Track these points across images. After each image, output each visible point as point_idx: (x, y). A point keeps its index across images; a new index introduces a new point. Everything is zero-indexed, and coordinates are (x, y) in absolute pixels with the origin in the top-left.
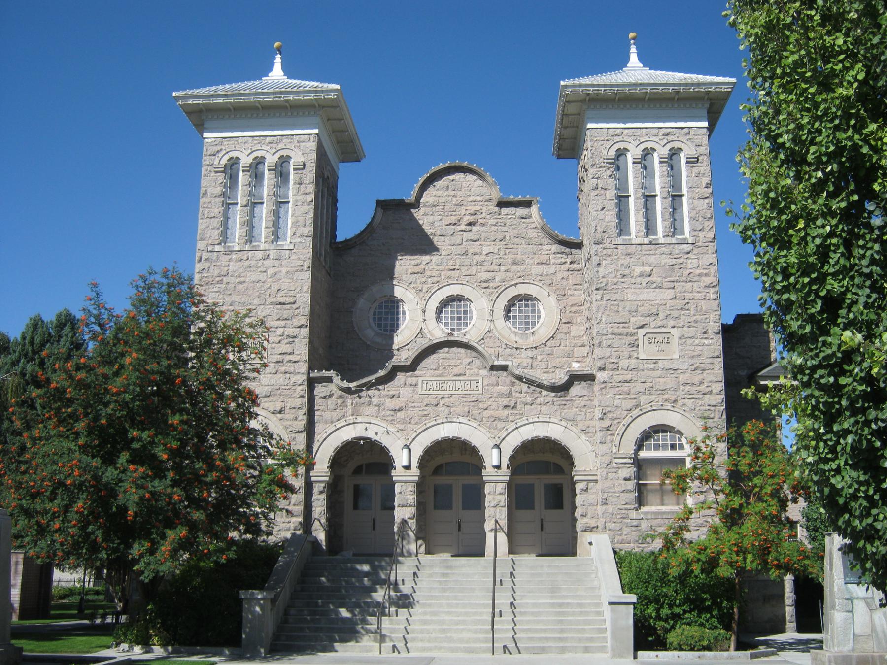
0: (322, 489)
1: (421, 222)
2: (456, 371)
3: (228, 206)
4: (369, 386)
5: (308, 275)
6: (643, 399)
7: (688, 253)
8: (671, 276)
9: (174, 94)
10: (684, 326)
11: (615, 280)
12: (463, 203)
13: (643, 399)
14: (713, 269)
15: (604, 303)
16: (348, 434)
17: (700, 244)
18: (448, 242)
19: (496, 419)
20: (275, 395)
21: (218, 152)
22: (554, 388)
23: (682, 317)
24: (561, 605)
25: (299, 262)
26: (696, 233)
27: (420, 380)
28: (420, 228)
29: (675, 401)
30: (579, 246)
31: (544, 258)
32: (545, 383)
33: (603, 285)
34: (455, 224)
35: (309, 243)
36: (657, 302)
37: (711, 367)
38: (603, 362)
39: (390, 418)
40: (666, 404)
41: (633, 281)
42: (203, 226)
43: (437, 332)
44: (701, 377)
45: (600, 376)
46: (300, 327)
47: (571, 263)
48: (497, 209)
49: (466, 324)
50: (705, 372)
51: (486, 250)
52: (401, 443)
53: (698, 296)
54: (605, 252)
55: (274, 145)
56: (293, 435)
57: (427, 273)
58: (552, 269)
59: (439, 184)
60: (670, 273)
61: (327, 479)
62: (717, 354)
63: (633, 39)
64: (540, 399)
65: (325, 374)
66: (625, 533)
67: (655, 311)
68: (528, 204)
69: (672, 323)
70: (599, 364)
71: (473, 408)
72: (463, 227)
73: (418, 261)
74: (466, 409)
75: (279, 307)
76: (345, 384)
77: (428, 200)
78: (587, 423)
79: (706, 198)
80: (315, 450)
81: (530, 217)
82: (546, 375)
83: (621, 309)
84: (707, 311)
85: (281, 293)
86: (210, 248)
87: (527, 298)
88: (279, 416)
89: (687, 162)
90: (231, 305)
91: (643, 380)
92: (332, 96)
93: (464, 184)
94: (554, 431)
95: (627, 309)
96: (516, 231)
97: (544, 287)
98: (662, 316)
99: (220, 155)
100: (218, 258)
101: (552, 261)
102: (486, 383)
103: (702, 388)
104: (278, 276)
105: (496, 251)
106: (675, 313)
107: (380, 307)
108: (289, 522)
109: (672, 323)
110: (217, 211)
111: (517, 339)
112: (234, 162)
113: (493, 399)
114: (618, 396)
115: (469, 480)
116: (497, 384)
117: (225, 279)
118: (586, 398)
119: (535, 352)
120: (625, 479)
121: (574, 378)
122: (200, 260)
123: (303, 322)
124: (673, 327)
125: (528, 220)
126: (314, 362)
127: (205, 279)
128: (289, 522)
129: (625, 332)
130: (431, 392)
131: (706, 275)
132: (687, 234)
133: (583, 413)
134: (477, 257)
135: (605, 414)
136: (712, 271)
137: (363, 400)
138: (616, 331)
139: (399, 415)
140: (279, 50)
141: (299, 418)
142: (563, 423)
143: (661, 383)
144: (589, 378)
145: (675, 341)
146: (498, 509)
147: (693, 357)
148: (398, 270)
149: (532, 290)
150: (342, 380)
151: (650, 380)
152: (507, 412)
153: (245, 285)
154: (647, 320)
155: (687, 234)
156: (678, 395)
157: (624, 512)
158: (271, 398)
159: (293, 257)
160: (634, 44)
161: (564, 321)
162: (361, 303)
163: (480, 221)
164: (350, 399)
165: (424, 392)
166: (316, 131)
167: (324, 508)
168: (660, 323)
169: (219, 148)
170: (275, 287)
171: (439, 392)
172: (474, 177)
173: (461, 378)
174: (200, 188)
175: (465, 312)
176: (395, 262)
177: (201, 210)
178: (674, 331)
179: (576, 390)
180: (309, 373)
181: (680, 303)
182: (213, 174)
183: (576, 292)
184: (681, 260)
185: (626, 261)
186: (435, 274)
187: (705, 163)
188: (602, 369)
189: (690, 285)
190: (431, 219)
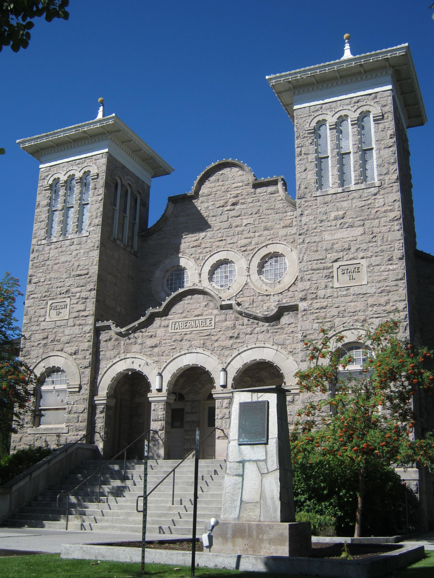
0: (101, 409)
1: (199, 208)
2: (196, 313)
3: (51, 212)
4: (135, 330)
6: (337, 321)
7: (375, 195)
8: (360, 216)
10: (371, 257)
11: (314, 226)
12: (229, 189)
13: (337, 321)
15: (306, 245)
16: (121, 367)
17: (385, 186)
18: (218, 220)
19: (224, 348)
20: (73, 342)
21: (47, 176)
22: (267, 319)
23: (371, 249)
25: (92, 244)
26: (381, 177)
27: (171, 321)
28: (198, 213)
29: (365, 321)
31: (288, 222)
32: (260, 315)
33: (305, 230)
34: (223, 206)
35: (99, 229)
36: (349, 239)
37: (395, 288)
38: (303, 293)
40: (357, 323)
44: (387, 298)
45: (302, 305)
46: (91, 290)
48: (253, 190)
50: (391, 293)
51: (245, 222)
52: (156, 371)
53: (384, 229)
54: (307, 204)
55: (80, 166)
56: (83, 370)
57: (203, 246)
59: (212, 179)
60: (359, 213)
61: (105, 402)
62: (400, 276)
63: (347, 39)
64: (258, 329)
65: (106, 323)
67: (346, 246)
68: (275, 183)
70: (301, 295)
71: (207, 342)
72: (229, 208)
73: (197, 237)
74: (202, 342)
75: (78, 278)
76: (119, 330)
77: (204, 191)
78: (294, 346)
79: (390, 147)
80: (99, 381)
84: (392, 241)
85: (80, 268)
86: (39, 243)
87: (276, 255)
88: (74, 356)
90: (50, 281)
91: (337, 305)
93: (230, 176)
94: (267, 354)
95: (324, 248)
96: (267, 205)
97: (288, 245)
98: (353, 250)
100: (43, 249)
102: (217, 320)
103: (388, 308)
104: (79, 256)
105: (252, 222)
106: (364, 246)
107: (172, 275)
108: (77, 435)
109: (361, 254)
110: (44, 216)
111: (267, 288)
112: (57, 180)
114: (317, 321)
116: (226, 320)
117: (47, 263)
118: (293, 325)
119: (281, 296)
121: (282, 310)
122: (33, 252)
123: (92, 287)
124: (363, 258)
126: (99, 316)
128: (77, 435)
129: (322, 267)
130: (178, 330)
131: (391, 211)
133: (291, 338)
134: (238, 229)
135: (305, 336)
136: (396, 207)
137: (133, 340)
138: (315, 267)
139: (156, 350)
140: (102, 103)
141: (87, 357)
142: (275, 347)
143: (352, 307)
144: (294, 308)
146: (224, 420)
147: (380, 282)
148: (183, 246)
149: (278, 248)
150: (117, 326)
151: (343, 305)
152: (232, 341)
153: (58, 265)
154: (341, 254)
158: (70, 344)
159: (89, 241)
160: (348, 42)
162: (158, 274)
163: (241, 201)
164: (123, 341)
165: (173, 331)
166: (106, 150)
167: (103, 424)
168: (351, 256)
170: (77, 264)
171: (183, 330)
172: (237, 169)
174: (36, 202)
175: (231, 272)
176: (181, 241)
177: (35, 217)
178: (364, 262)
179: (285, 319)
180: (95, 324)
181: (368, 237)
182: (44, 192)
184: (369, 202)
186: (208, 245)
188: (304, 299)
189: (377, 221)
190: (206, 205)
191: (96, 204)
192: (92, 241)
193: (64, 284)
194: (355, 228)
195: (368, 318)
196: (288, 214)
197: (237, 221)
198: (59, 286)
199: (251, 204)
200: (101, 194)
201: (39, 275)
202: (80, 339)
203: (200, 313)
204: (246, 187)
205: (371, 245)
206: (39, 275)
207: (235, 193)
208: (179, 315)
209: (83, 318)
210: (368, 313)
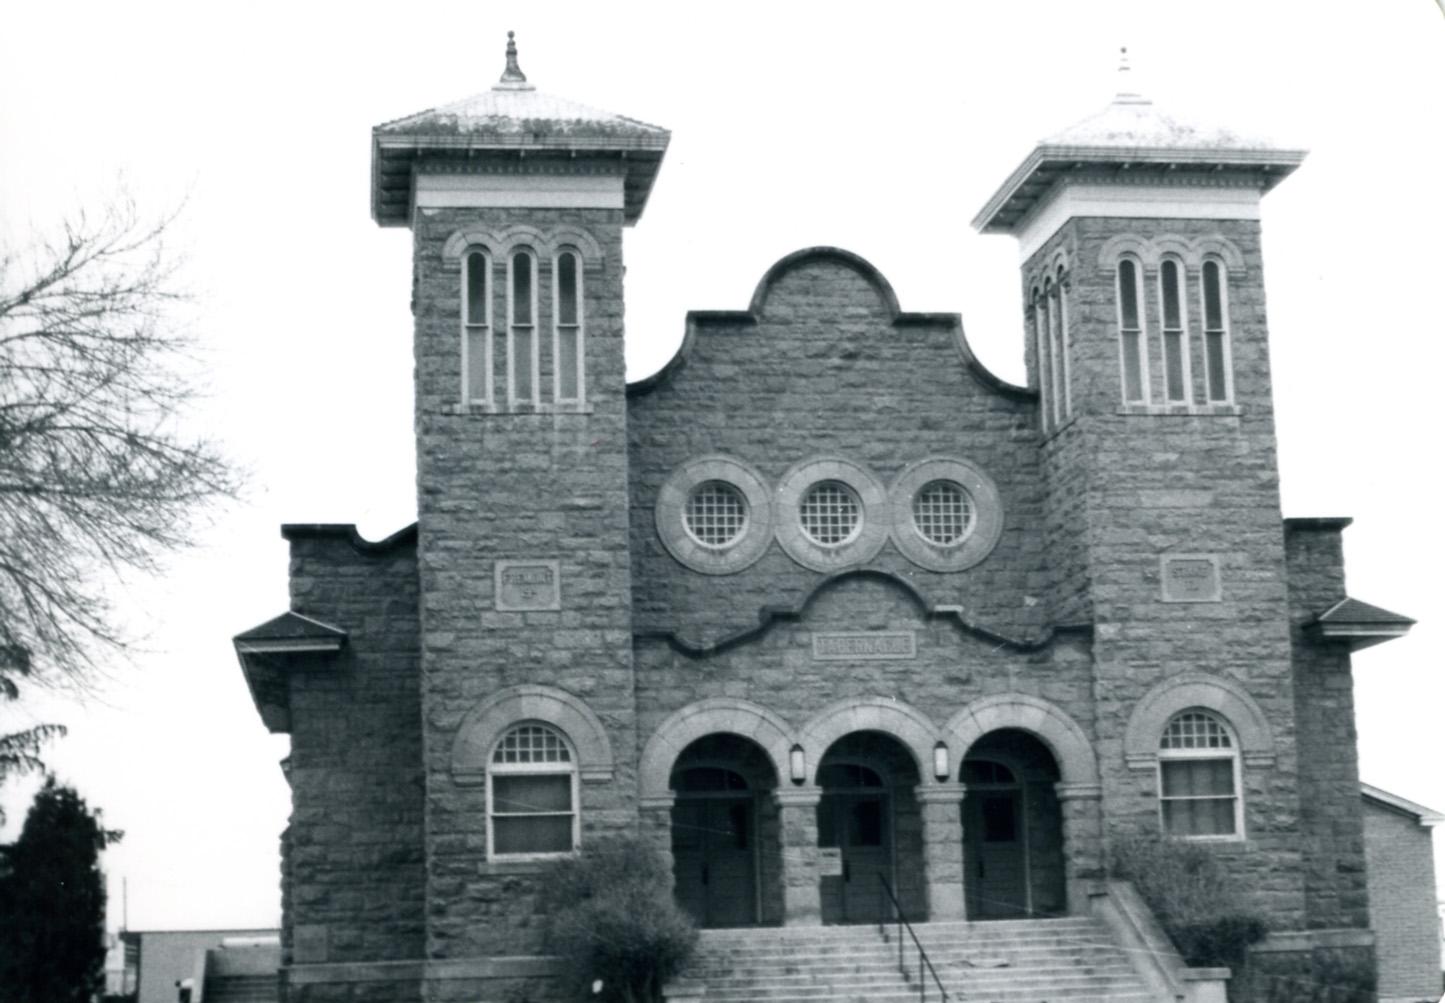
2: (874, 620)
22: (1026, 649)
27: (815, 636)
31: (976, 418)
48: (894, 332)
58: (988, 439)
69: (1212, 545)
72: (836, 361)
75: (576, 514)
86: (446, 409)
94: (1031, 716)
99: (453, 238)
101: (989, 423)
123: (618, 538)
125: (946, 352)
127: (440, 464)
145: (1217, 574)
154: (1174, 540)
173: (881, 633)
178: (1214, 558)
209: (600, 612)
210: (1224, 656)
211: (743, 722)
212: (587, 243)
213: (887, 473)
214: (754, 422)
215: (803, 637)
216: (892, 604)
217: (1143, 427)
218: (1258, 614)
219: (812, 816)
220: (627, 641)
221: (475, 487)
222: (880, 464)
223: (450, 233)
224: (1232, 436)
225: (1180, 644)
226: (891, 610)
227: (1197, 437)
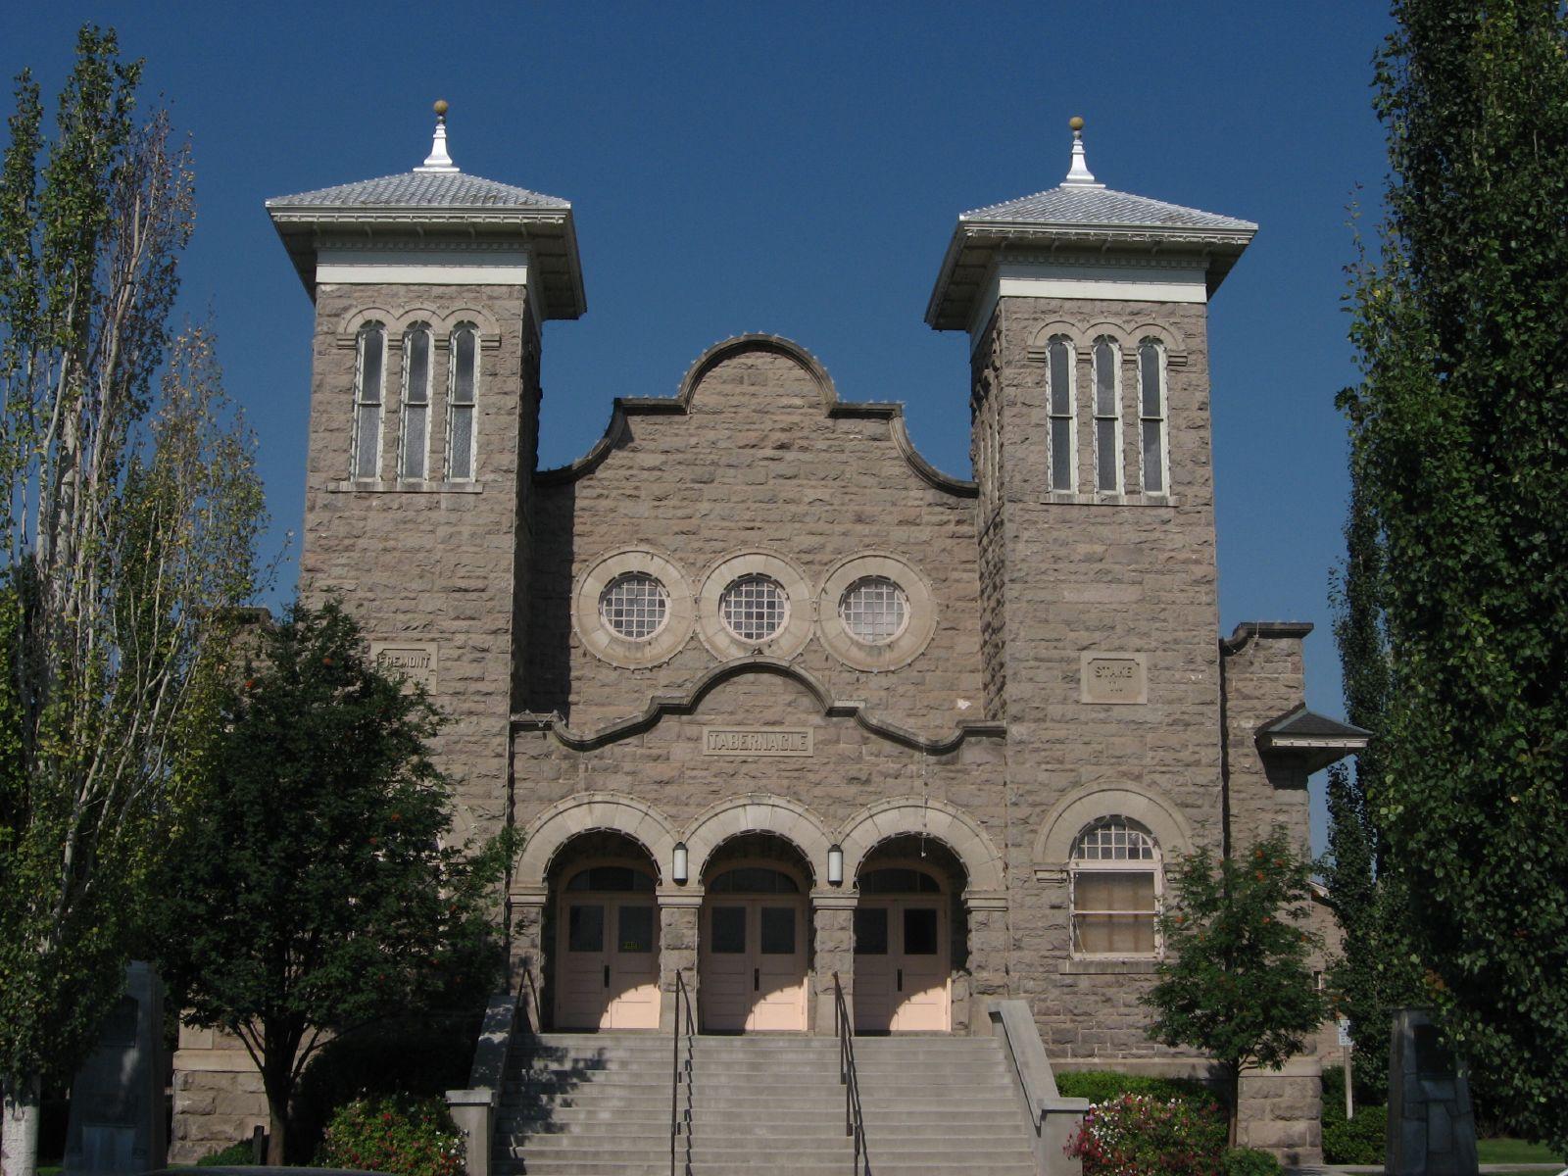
2: (769, 715)
5: (508, 543)
8: (1137, 563)
9: (268, 203)
11: (1043, 566)
12: (769, 408)
14: (1211, 552)
15: (1024, 604)
16: (578, 820)
17: (1187, 508)
19: (839, 801)
22: (935, 749)
24: (954, 1116)
25: (493, 517)
26: (1179, 489)
27: (706, 730)
30: (973, 493)
31: (911, 513)
36: (1114, 606)
37: (1199, 719)
39: (653, 795)
41: (1072, 567)
42: (320, 445)
43: (727, 643)
47: (959, 522)
48: (830, 422)
49: (772, 627)
51: (811, 494)
52: (669, 841)
54: (1027, 517)
58: (925, 533)
64: (912, 768)
66: (1052, 997)
68: (886, 415)
69: (1137, 642)
71: (795, 781)
72: (769, 452)
75: (457, 595)
77: (706, 400)
81: (888, 439)
82: (911, 721)
83: (1051, 617)
86: (332, 486)
89: (1170, 364)
91: (1086, 739)
92: (557, 220)
94: (936, 822)
98: (1119, 629)
99: (348, 316)
101: (926, 518)
105: (826, 498)
109: (1137, 642)
113: (831, 766)
114: (1044, 766)
115: (780, 901)
118: (988, 767)
120: (1053, 907)
127: (322, 542)
131: (1197, 562)
132: (1166, 491)
134: (793, 508)
138: (1044, 654)
139: (669, 790)
142: (950, 809)
145: (1143, 673)
152: (854, 789)
153: (396, 554)
154: (1097, 636)
155: (1166, 491)
156: (1144, 767)
157: (1050, 961)
160: (1080, 137)
161: (945, 625)
168: (1117, 643)
169: (345, 302)
172: (790, 363)
173: (777, 729)
175: (771, 605)
178: (1141, 658)
179: (973, 753)
182: (335, 351)
183: (965, 576)
184: (1156, 535)
185: (1063, 533)
187: (1199, 366)
191: (497, 413)
192: (492, 510)
193: (417, 606)
194: (1123, 586)
195: (1146, 771)
196: (912, 493)
197: (788, 489)
198: (403, 608)
199: (824, 454)
200: (513, 392)
201: (338, 571)
202: (475, 748)
203: (776, 718)
204: (811, 411)
205: (1158, 625)
206: (338, 571)
207: (787, 419)
208: (725, 716)
209: (477, 698)
210: (1148, 761)
211: (625, 819)
212: (486, 319)
213: (816, 567)
214: (680, 513)
215: (692, 731)
216: (789, 698)
217: (1068, 517)
218: (1186, 717)
219: (694, 919)
220: (503, 728)
221: (356, 567)
222: (809, 557)
223: (346, 309)
224: (1166, 527)
225: (1099, 747)
226: (789, 704)
227: (1127, 527)
